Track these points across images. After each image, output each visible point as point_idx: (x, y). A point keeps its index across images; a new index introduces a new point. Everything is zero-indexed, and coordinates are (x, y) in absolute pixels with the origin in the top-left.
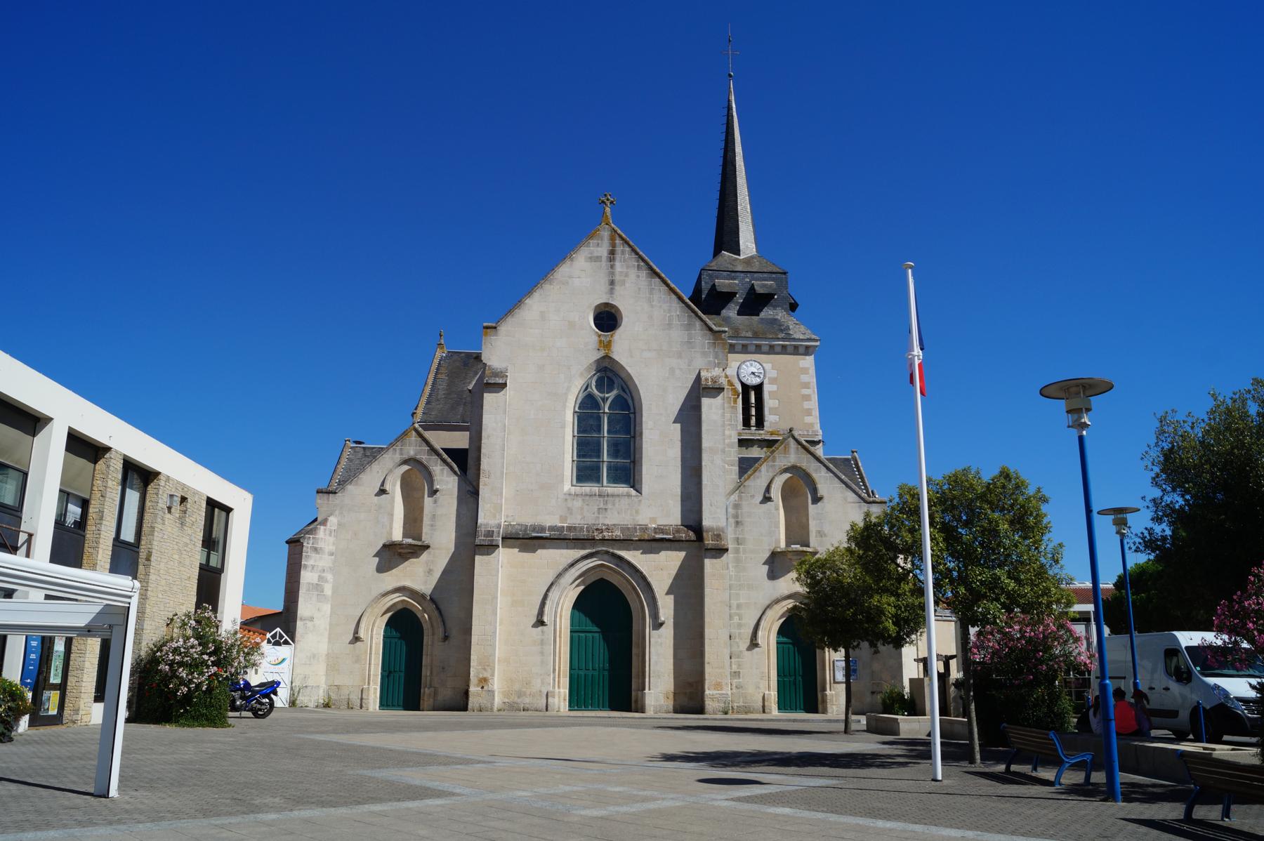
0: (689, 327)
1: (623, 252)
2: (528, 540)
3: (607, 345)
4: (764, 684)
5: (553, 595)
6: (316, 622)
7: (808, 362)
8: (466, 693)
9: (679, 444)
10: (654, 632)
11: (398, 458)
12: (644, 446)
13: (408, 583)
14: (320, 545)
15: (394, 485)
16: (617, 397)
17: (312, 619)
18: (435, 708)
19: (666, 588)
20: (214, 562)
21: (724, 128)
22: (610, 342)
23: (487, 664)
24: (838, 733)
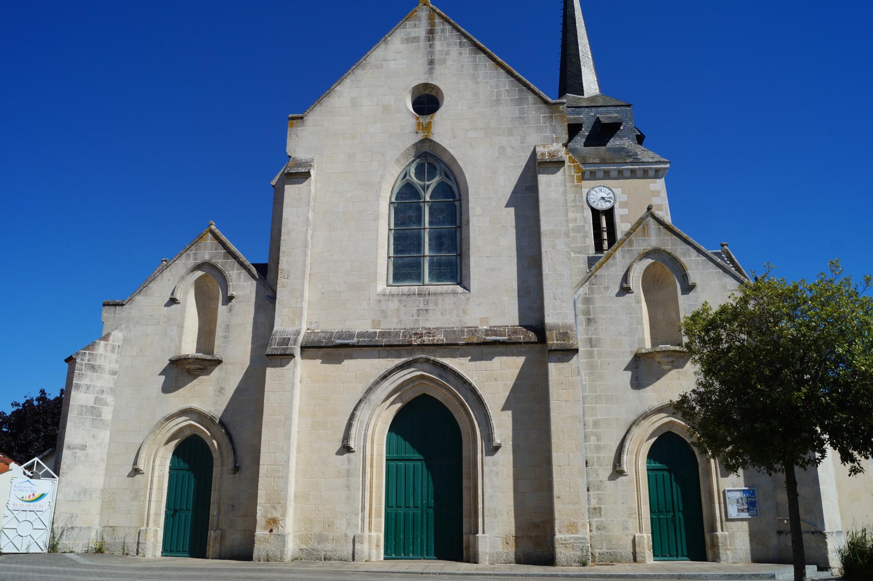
0: (520, 101)
1: (443, 31)
2: (331, 349)
3: (428, 127)
4: (633, 524)
5: (363, 414)
6: (90, 451)
7: (659, 185)
9: (513, 231)
10: (488, 459)
11: (191, 263)
12: (471, 235)
13: (196, 405)
14: (98, 362)
15: (186, 293)
16: (440, 185)
17: (83, 447)
18: (221, 557)
19: (502, 402)
22: (430, 123)
23: (278, 501)
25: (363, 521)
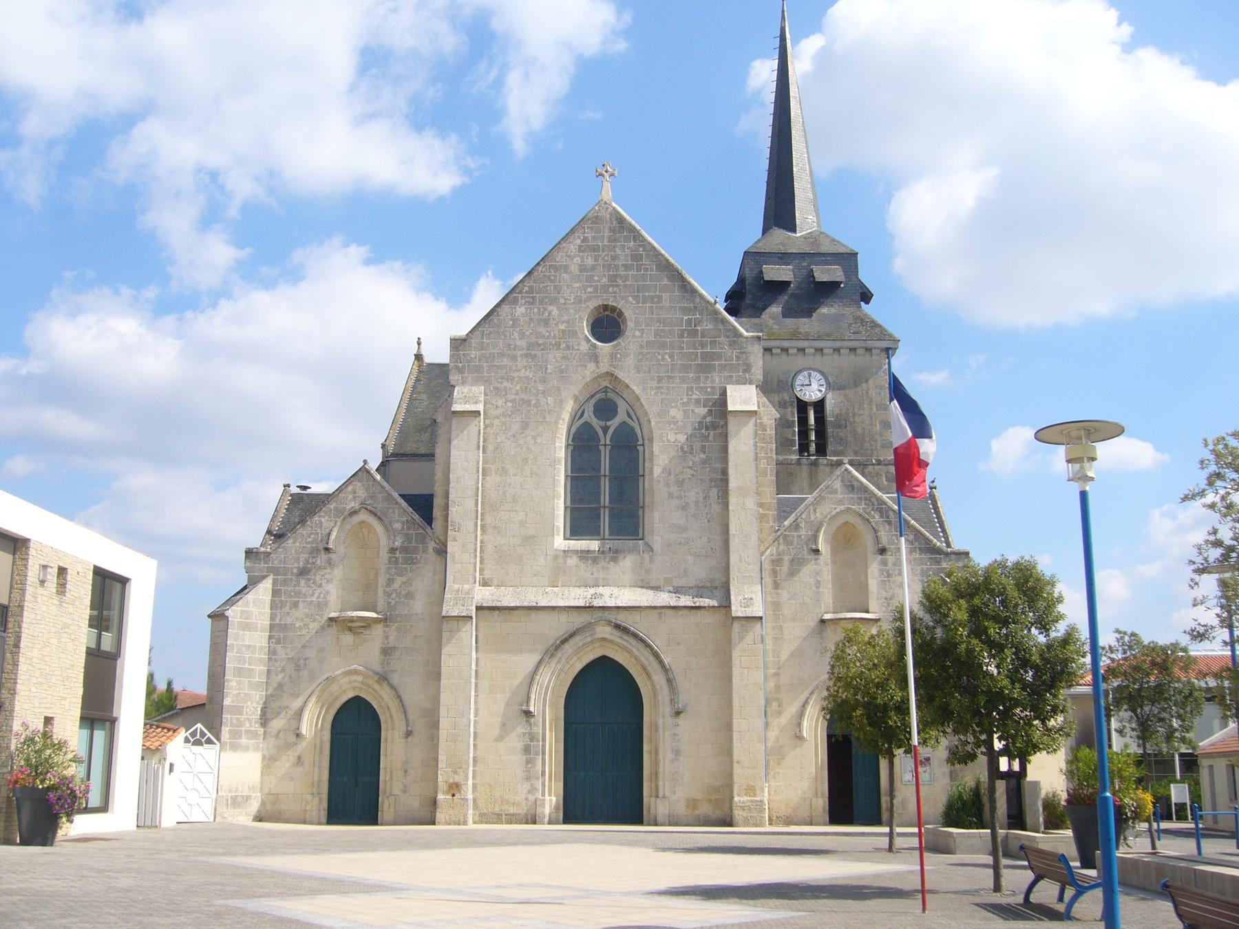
8: (434, 802)
20: (107, 645)
21: (777, 43)
24: (231, 601)
25: (543, 785)
